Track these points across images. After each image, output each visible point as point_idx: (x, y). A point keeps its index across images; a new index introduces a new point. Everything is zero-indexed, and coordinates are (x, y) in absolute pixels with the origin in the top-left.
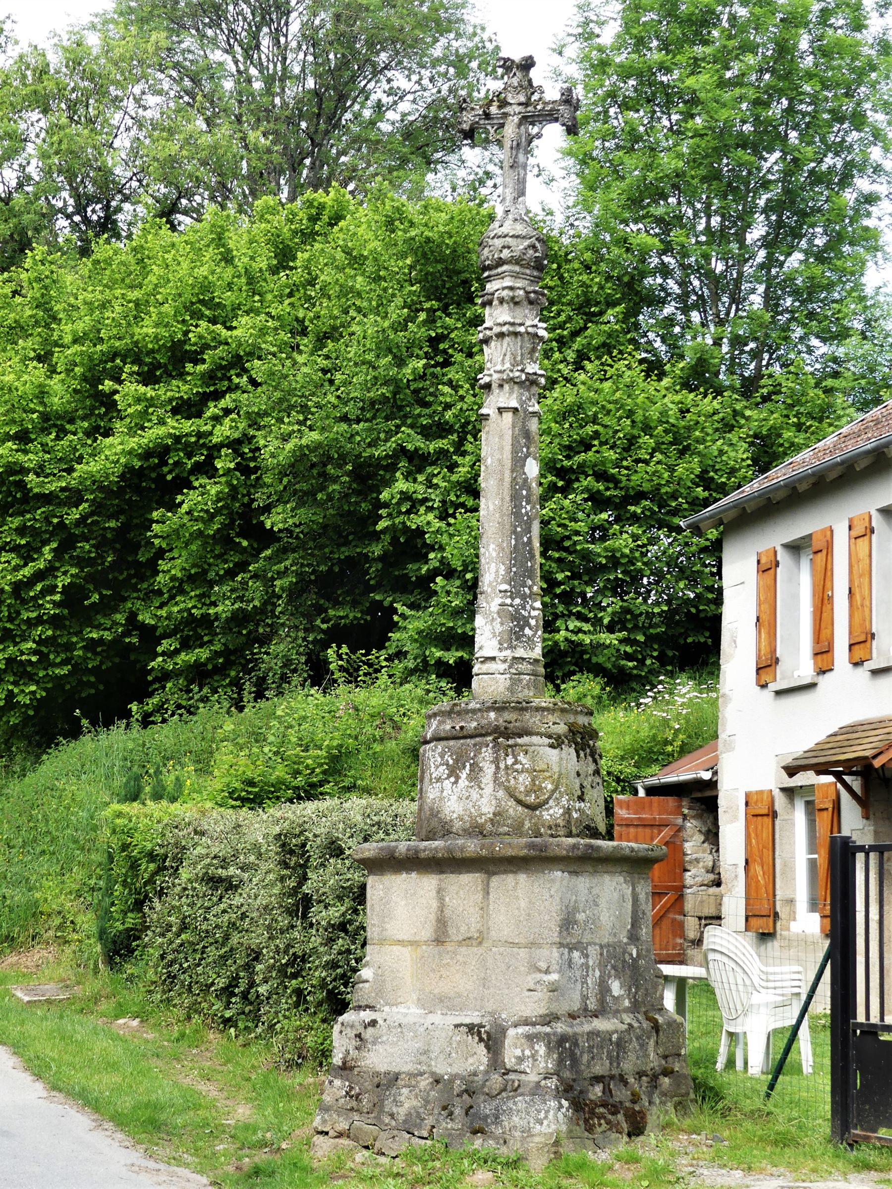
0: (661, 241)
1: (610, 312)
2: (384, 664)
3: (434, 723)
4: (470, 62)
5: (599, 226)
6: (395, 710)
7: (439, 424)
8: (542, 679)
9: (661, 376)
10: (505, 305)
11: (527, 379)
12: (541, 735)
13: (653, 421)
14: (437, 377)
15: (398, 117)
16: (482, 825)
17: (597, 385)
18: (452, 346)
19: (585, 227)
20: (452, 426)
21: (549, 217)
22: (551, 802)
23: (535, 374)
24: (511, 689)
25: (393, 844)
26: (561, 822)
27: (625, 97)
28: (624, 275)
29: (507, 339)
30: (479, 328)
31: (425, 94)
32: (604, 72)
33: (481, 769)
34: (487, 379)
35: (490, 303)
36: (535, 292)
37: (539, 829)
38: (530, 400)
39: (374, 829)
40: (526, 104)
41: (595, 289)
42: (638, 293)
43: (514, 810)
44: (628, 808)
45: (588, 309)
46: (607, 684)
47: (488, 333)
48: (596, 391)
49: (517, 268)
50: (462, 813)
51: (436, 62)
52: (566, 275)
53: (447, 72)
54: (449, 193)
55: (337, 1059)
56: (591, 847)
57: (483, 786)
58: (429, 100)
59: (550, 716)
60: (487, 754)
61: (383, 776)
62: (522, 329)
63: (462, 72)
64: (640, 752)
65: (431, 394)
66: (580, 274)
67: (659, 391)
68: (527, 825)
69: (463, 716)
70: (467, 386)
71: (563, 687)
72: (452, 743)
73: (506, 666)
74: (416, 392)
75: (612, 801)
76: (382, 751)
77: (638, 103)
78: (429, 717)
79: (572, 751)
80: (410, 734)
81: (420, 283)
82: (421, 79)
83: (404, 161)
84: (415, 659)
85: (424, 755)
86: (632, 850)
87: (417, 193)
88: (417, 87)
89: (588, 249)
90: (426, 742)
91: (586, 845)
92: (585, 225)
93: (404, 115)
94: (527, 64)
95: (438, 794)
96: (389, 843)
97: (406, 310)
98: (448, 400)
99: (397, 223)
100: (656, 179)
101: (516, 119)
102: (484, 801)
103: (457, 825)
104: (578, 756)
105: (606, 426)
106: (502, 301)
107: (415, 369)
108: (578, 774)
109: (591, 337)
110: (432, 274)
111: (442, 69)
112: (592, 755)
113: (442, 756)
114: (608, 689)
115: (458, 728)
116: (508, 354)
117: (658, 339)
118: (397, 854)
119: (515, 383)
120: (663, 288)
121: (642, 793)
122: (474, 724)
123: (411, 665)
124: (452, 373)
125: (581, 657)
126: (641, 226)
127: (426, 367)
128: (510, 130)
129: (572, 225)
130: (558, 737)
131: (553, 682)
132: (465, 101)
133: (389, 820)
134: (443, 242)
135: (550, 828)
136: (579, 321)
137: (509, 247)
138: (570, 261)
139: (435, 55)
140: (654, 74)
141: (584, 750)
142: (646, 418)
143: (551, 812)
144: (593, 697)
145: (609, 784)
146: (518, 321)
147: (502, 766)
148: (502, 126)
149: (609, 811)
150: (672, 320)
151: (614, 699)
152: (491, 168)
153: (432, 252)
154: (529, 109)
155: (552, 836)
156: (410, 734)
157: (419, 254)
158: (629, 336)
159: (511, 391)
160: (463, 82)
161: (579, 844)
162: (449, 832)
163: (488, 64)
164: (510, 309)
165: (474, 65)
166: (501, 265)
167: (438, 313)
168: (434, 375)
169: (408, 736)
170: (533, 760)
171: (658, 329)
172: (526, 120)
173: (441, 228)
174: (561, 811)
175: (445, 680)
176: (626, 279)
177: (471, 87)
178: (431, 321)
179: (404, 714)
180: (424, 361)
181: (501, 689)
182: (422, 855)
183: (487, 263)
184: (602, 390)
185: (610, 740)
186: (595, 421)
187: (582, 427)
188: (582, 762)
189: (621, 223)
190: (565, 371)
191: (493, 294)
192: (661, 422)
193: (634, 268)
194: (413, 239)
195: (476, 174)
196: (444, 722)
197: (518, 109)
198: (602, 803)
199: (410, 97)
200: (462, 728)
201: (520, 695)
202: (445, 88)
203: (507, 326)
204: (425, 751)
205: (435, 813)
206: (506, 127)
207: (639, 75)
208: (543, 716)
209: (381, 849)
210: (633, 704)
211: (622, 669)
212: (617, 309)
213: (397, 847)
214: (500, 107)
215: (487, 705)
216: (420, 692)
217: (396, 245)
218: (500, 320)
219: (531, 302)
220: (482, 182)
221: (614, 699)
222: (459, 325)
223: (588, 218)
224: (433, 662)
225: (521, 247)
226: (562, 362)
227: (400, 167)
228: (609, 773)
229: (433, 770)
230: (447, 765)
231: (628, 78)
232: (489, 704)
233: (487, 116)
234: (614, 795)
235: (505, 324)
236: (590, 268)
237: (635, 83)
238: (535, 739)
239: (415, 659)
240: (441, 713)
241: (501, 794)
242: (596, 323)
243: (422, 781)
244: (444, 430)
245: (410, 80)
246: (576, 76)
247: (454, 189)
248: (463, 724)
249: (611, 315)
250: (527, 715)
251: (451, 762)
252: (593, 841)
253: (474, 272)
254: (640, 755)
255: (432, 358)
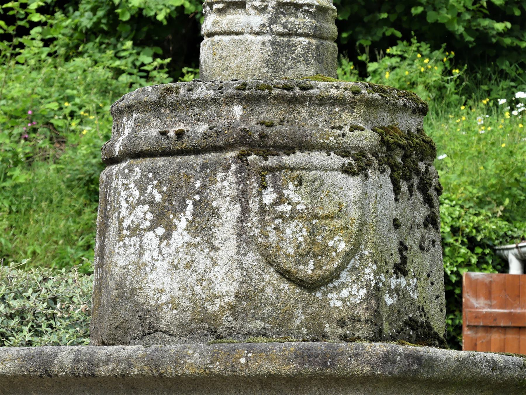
2: (36, 18)
3: (128, 125)
6: (54, 106)
8: (333, 46)
12: (327, 149)
16: (215, 317)
22: (344, 274)
24: (273, 63)
25: (49, 349)
26: (363, 313)
33: (214, 213)
37: (321, 326)
39: (13, 323)
43: (275, 289)
44: (489, 296)
46: (455, 63)
50: (177, 293)
55: (30, 198)
56: (418, 359)
57: (217, 243)
59: (346, 115)
60: (226, 183)
61: (32, 230)
64: (515, 191)
68: (299, 317)
69: (183, 113)
71: (372, 67)
72: (160, 162)
73: (264, 18)
75: (459, 283)
76: (31, 183)
78: (119, 113)
79: (386, 179)
80: (83, 150)
84: (94, 10)
85: (108, 185)
86: (494, 365)
90: (112, 161)
91: (408, 356)
95: (134, 257)
96: (44, 346)
102: (220, 271)
103: (169, 317)
104: (397, 191)
108: (396, 224)
112: (424, 188)
113: (142, 186)
114: (456, 72)
115: (172, 134)
118: (55, 369)
121: (515, 268)
122: (203, 128)
123: (86, 21)
125: (407, 12)
130: (361, 155)
131: (353, 58)
133: (41, 307)
135: (342, 323)
141: (407, 179)
143: (345, 293)
144: (427, 87)
145: (455, 250)
147: (254, 206)
149: (453, 301)
151: (468, 92)
155: (345, 338)
156: (83, 150)
161: (394, 353)
162: (153, 329)
169: (80, 155)
170: (312, 195)
174: (363, 292)
175: (150, 51)
179: (72, 114)
181: (255, 62)
182: (102, 371)
185: (459, 168)
188: (403, 202)
196: (147, 123)
198: (440, 286)
200: (180, 134)
201: (290, 75)
204: (109, 177)
205: (127, 294)
208: (332, 115)
209: (26, 358)
210: (502, 101)
211: (482, 36)
213: (55, 355)
215: (228, 91)
216: (102, 73)
221: (468, 92)
224: (126, 17)
228: (455, 231)
229: (124, 212)
230: (152, 203)
232: (231, 90)
234: (464, 272)
238: (317, 157)
239: (94, 10)
240: (140, 106)
241: (251, 258)
243: (103, 233)
248: (181, 127)
250: (304, 112)
251: (158, 198)
252: (421, 349)
254: (513, 197)
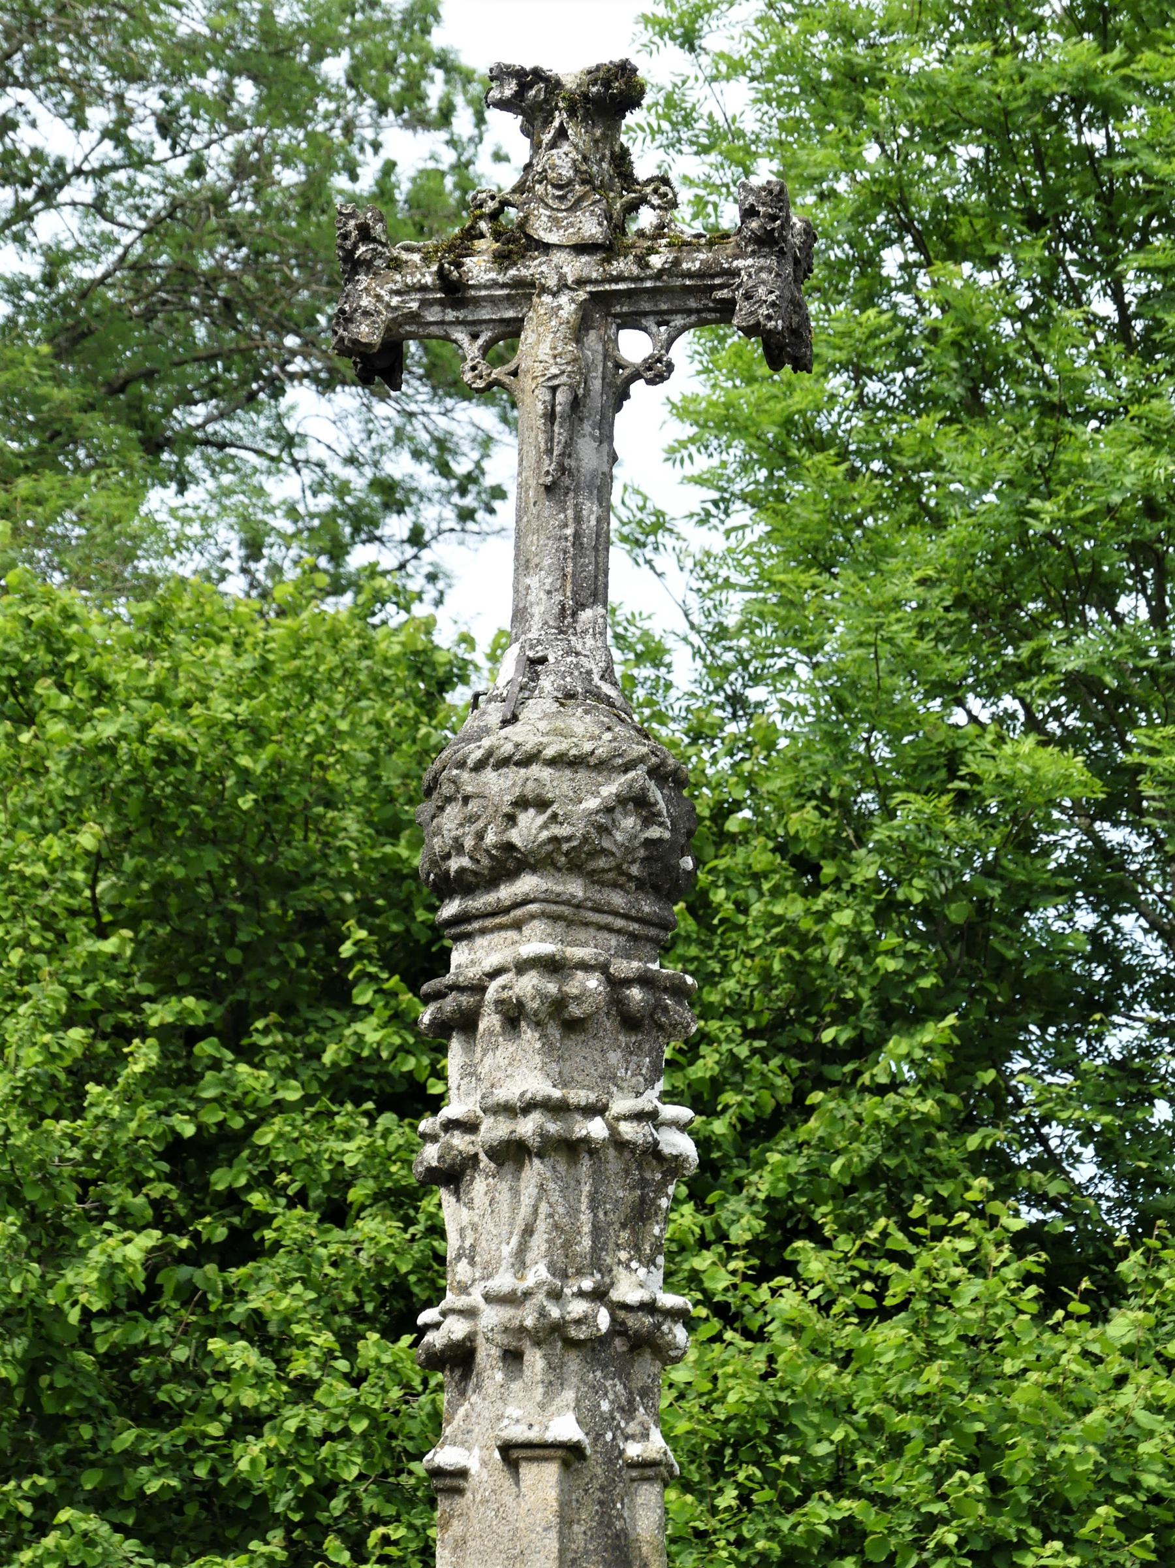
0: (1095, 765)
1: (898, 1045)
4: (318, 56)
5: (847, 700)
7: (208, 1494)
9: (1109, 1295)
10: (529, 1034)
11: (618, 1328)
13: (1076, 1479)
14: (204, 1303)
15: (33, 267)
17: (848, 1335)
18: (265, 1180)
19: (787, 709)
20: (263, 1501)
21: (645, 672)
23: (649, 1307)
27: (941, 204)
28: (947, 898)
29: (534, 1170)
30: (426, 1124)
31: (143, 180)
32: (860, 113)
34: (457, 1328)
35: (467, 1023)
36: (645, 980)
38: (629, 1411)
40: (606, 249)
41: (836, 953)
42: (1002, 969)
45: (809, 1034)
47: (460, 1141)
48: (846, 1360)
49: (575, 888)
51: (186, 56)
52: (719, 895)
53: (228, 95)
54: (232, 564)
58: (159, 202)
62: (596, 1128)
63: (288, 95)
65: (180, 1373)
66: (777, 892)
67: (1098, 1360)
70: (325, 1339)
74: (120, 1360)
77: (993, 230)
81: (133, 921)
82: (124, 122)
83: (57, 436)
87: (109, 562)
88: (109, 151)
89: (801, 794)
92: (789, 703)
93: (56, 260)
94: (613, 94)
97: (77, 1034)
98: (249, 1398)
99: (44, 687)
100: (1065, 523)
101: (567, 305)
105: (884, 1502)
106: (514, 1016)
107: (112, 1268)
109: (827, 1149)
110: (181, 887)
111: (210, 82)
116: (542, 1226)
117: (1089, 1152)
119: (572, 1344)
120: (1102, 949)
124: (268, 1292)
126: (1009, 703)
127: (156, 1261)
128: (542, 346)
129: (736, 701)
132: (365, 233)
134: (229, 761)
136: (776, 1077)
137: (542, 804)
138: (732, 838)
139: (183, 31)
140: (1054, 118)
142: (1049, 1469)
146: (580, 1096)
148: (512, 330)
150: (1139, 1075)
152: (399, 466)
153: (185, 800)
154: (621, 266)
157: (133, 808)
158: (973, 1142)
159: (555, 1380)
160: (288, 136)
163: (389, 66)
164: (548, 1048)
165: (335, 68)
166: (512, 875)
167: (207, 1048)
168: (191, 1296)
171: (1085, 1113)
172: (604, 309)
173: (220, 708)
176: (957, 913)
177: (325, 158)
178: (177, 1077)
180: (151, 1238)
183: (454, 864)
184: (870, 1356)
186: (840, 1483)
187: (792, 1505)
189: (929, 695)
190: (719, 1282)
191: (478, 989)
192: (1107, 1486)
193: (990, 871)
194: (109, 749)
195: (342, 489)
197: (573, 267)
199: (82, 191)
202: (219, 158)
203: (536, 1117)
206: (528, 336)
207: (997, 127)
212: (930, 1033)
214: (502, 259)
217: (38, 772)
218: (509, 1092)
219: (630, 1022)
220: (364, 524)
222: (293, 1095)
223: (803, 671)
225: (592, 803)
226: (704, 1244)
227: (39, 462)
231: (956, 135)
233: (453, 291)
235: (528, 1107)
236: (816, 870)
237: (978, 152)
242: (845, 1087)
244: (233, 1516)
245: (81, 124)
246: (749, 125)
247: (253, 549)
249: (897, 1055)
253: (350, 881)
255: (179, 1226)
